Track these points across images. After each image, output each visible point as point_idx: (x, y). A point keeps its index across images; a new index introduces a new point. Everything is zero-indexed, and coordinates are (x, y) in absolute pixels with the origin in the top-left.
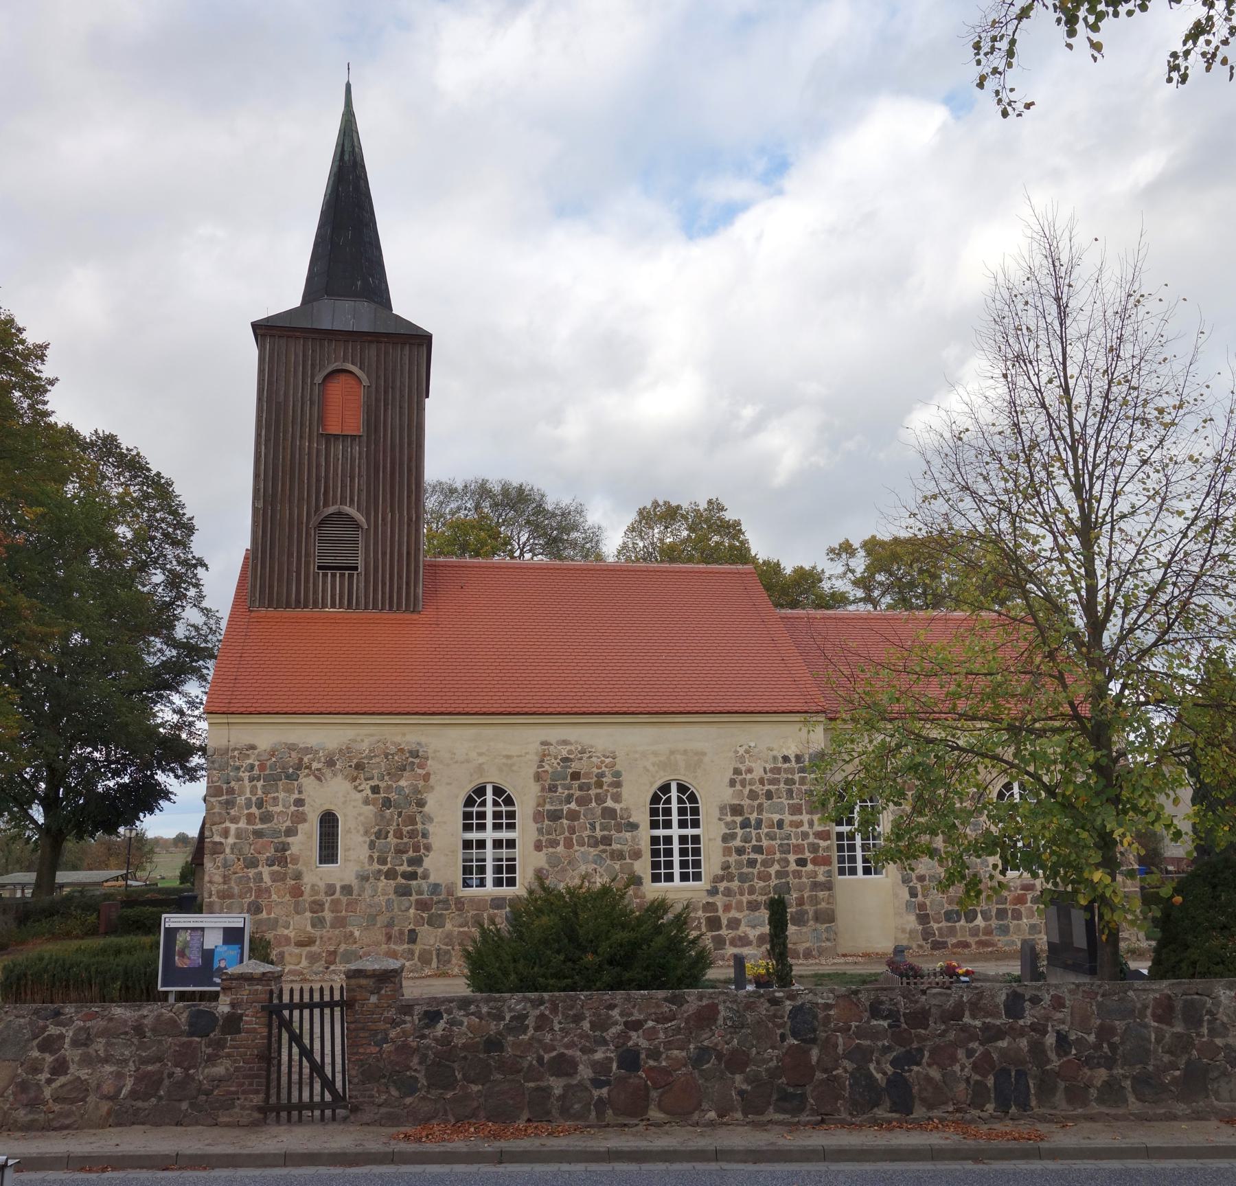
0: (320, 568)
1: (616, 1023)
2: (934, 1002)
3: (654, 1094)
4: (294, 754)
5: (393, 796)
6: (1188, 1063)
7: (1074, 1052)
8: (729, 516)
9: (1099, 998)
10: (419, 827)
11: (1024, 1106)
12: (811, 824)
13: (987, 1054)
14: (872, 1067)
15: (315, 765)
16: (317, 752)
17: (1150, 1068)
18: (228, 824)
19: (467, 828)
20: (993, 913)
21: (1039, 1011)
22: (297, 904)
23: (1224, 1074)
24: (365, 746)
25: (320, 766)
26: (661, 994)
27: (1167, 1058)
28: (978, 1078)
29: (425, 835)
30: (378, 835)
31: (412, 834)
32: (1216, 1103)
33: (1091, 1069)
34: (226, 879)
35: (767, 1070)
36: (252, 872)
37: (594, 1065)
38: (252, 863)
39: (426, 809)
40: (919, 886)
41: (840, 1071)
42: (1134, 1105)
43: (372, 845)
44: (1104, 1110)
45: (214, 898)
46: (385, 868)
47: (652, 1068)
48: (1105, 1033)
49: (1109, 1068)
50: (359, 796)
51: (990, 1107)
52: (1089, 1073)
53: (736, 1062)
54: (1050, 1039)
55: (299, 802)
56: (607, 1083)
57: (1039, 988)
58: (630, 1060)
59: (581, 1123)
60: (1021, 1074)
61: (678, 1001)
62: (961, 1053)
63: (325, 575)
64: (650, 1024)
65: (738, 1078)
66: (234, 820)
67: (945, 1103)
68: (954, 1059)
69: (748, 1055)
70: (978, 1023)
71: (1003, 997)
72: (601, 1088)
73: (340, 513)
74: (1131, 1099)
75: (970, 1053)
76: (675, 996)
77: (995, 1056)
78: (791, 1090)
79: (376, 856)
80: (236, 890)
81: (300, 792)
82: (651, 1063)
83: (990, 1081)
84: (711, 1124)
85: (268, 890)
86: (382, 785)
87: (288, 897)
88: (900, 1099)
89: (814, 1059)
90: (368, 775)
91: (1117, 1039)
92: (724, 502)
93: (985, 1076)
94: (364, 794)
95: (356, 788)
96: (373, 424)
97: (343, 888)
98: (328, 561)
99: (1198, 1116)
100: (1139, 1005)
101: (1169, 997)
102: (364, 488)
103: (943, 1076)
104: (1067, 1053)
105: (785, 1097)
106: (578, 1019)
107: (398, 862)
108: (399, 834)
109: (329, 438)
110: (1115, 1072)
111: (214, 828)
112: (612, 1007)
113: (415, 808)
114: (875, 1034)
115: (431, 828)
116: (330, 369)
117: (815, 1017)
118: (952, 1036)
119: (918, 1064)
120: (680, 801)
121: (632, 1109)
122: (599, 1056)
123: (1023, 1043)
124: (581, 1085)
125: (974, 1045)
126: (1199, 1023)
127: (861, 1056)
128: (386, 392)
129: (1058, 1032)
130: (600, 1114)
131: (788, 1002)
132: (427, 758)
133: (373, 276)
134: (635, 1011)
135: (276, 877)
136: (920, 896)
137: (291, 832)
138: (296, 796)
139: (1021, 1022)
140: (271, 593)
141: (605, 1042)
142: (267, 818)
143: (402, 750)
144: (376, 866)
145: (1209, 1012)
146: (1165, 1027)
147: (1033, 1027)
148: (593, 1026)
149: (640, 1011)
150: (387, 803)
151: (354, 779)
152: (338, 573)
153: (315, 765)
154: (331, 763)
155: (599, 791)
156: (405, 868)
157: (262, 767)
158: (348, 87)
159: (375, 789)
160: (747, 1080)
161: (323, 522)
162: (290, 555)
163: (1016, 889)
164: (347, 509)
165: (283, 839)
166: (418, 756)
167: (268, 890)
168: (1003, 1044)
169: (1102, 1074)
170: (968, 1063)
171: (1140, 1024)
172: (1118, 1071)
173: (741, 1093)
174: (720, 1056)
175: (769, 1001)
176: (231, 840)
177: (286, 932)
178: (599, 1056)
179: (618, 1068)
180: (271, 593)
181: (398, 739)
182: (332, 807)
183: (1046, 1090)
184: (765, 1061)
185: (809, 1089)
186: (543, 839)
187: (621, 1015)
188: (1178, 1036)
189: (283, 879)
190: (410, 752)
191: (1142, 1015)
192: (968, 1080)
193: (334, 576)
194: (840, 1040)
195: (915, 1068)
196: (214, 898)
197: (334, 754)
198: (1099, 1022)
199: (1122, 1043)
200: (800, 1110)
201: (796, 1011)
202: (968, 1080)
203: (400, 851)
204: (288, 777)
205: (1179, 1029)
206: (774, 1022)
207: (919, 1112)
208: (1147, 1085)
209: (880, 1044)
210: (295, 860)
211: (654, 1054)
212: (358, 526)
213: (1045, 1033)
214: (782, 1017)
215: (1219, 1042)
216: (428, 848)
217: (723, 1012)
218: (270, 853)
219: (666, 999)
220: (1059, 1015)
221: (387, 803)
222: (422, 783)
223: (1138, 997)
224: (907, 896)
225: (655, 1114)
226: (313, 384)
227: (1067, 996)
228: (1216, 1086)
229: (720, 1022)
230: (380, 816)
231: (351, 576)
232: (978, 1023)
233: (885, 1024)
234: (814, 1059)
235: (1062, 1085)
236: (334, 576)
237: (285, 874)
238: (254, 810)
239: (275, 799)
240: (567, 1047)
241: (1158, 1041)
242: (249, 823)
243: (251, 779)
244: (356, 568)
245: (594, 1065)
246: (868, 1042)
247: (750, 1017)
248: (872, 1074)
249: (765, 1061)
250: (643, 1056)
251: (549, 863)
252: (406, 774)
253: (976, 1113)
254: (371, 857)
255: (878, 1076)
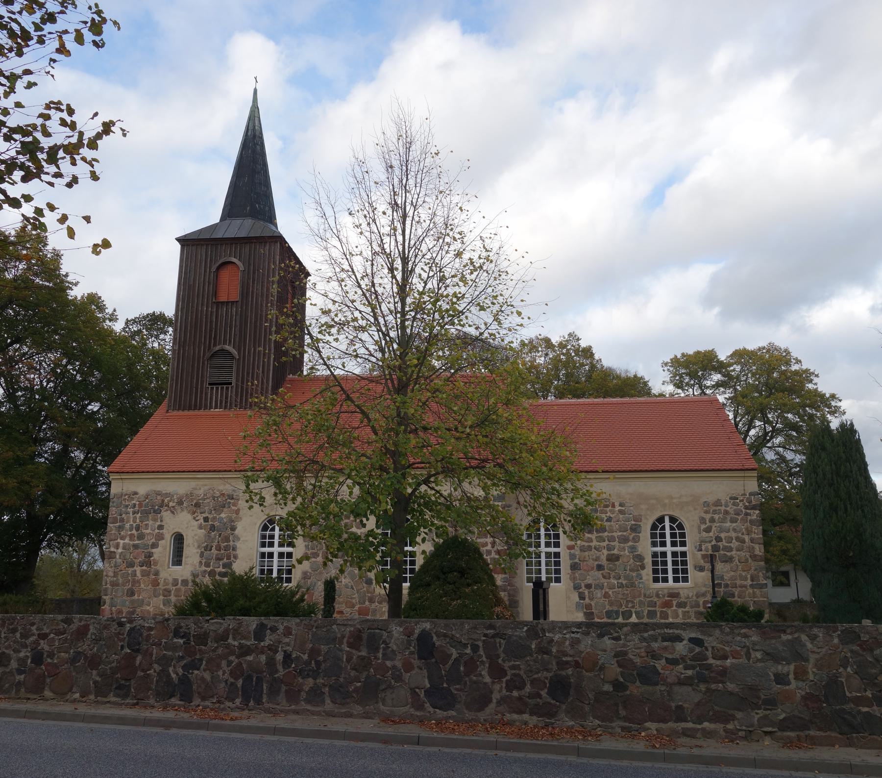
0: (210, 384)
1: (34, 635)
2: (212, 628)
3: (48, 680)
4: (159, 497)
5: (217, 524)
6: (367, 677)
7: (293, 665)
8: (583, 344)
9: (314, 630)
10: (231, 543)
11: (259, 702)
12: (493, 544)
13: (240, 664)
14: (171, 669)
15: (171, 504)
16: (173, 496)
17: (342, 680)
18: (119, 540)
19: (263, 545)
20: (645, 614)
21: (274, 637)
22: (155, 590)
23: (390, 687)
24: (201, 492)
25: (174, 504)
26: (60, 617)
27: (353, 673)
28: (232, 680)
29: (234, 549)
30: (206, 548)
31: (227, 548)
32: (382, 707)
33: (303, 678)
34: (115, 574)
35: (110, 668)
36: (130, 570)
37: (19, 660)
38: (131, 565)
39: (236, 532)
40: (586, 592)
41: (152, 671)
42: (329, 705)
43: (202, 555)
44: (309, 707)
45: (108, 586)
46: (209, 569)
47: (49, 664)
48: (314, 653)
49: (315, 679)
50: (196, 523)
51: (238, 701)
52: (301, 680)
53: (94, 662)
54: (279, 657)
55: (161, 527)
56: (24, 672)
57: (277, 621)
58: (38, 658)
59: (7, 696)
60: (260, 680)
61: (68, 621)
62: (224, 663)
63: (212, 389)
64: (52, 635)
65: (94, 672)
66: (123, 538)
67: (212, 697)
68: (219, 667)
69: (101, 658)
70: (236, 643)
71: (254, 626)
72: (21, 674)
73: (223, 350)
74: (328, 701)
75: (229, 663)
76: (67, 619)
77: (245, 666)
78: (123, 682)
79: (204, 561)
80: (121, 581)
81: (161, 521)
82: (49, 660)
83: (240, 683)
84: (74, 701)
85: (139, 582)
86: (210, 516)
87: (150, 586)
88: (184, 691)
89: (138, 662)
90: (202, 510)
91: (321, 658)
92: (579, 334)
93: (236, 679)
94: (199, 522)
95: (194, 518)
96: (245, 294)
97: (183, 581)
98: (214, 380)
99: (367, 716)
100: (339, 635)
101: (360, 631)
102: (238, 333)
103: (212, 678)
104: (290, 667)
105: (120, 687)
106: (14, 631)
107: (217, 565)
108: (219, 548)
109: (219, 304)
110: (318, 681)
111: (111, 543)
112: (33, 624)
113: (229, 532)
114: (175, 648)
115: (238, 544)
116: (220, 262)
117: (141, 635)
118: (220, 651)
119: (198, 669)
120: (672, 528)
121: (36, 688)
122: (22, 655)
123: (263, 658)
124: (11, 672)
125: (232, 658)
126: (377, 649)
127: (165, 662)
128: (254, 273)
129: (285, 652)
130: (18, 691)
131: (128, 625)
132: (238, 500)
133: (259, 204)
134: (45, 628)
135: (145, 574)
136: (587, 599)
137: (155, 546)
138: (159, 523)
139: (262, 644)
140: (180, 401)
141: (26, 646)
142: (141, 537)
143: (223, 495)
144: (203, 568)
145: (384, 642)
146: (354, 651)
147: (270, 648)
148: (22, 636)
149: (48, 628)
150: (213, 528)
151: (194, 513)
152: (220, 387)
153: (171, 504)
154: (180, 503)
155: (347, 521)
156: (221, 569)
157: (140, 505)
158: (255, 91)
159: (206, 519)
160: (98, 674)
161: (212, 356)
162: (192, 378)
163: (664, 596)
164: (227, 347)
165: (150, 550)
166: (233, 498)
167: (139, 582)
168: (250, 658)
169: (310, 682)
170: (228, 670)
171: (338, 649)
172: (320, 681)
173: (95, 682)
174: (86, 657)
175: (118, 624)
176: (120, 550)
177: (148, 608)
178: (22, 655)
179: (31, 662)
180: (180, 401)
181: (221, 488)
182: (180, 531)
183: (273, 692)
184: (110, 663)
185: (133, 682)
186: (309, 552)
187: (37, 630)
188: (362, 658)
189: (148, 575)
190: (228, 496)
191: (341, 643)
192: (226, 681)
193: (217, 389)
194: (155, 651)
195: (196, 672)
196: (108, 586)
197: (183, 497)
198: (311, 645)
199: (324, 661)
200: (126, 696)
201: (132, 630)
202: (226, 681)
203: (219, 559)
204: (155, 512)
205: (364, 653)
206: (118, 638)
207: (197, 701)
208: (341, 693)
209: (177, 654)
210: (156, 563)
211: (51, 655)
212: (233, 358)
213: (276, 652)
214: (123, 634)
215: (389, 663)
216: (236, 557)
217: (92, 629)
218: (141, 558)
219: (62, 621)
220: (287, 640)
221: (213, 528)
222: (234, 515)
223: (339, 630)
224: (577, 599)
225: (48, 693)
226: (210, 272)
227: (294, 627)
228: (383, 695)
229: (89, 636)
230: (208, 535)
231: (227, 388)
232: (236, 643)
233: (181, 641)
234: (138, 662)
235: (284, 688)
236: (217, 389)
237: (149, 572)
238: (134, 532)
239: (146, 525)
240: (6, 648)
241: (348, 661)
242: (131, 540)
243: (134, 513)
244: (231, 384)
245: (19, 660)
246: (170, 653)
247: (105, 634)
248: (170, 674)
249: (110, 663)
250: (45, 656)
251: (311, 568)
252: (225, 510)
253: (230, 704)
254: (201, 562)
255: (174, 676)
